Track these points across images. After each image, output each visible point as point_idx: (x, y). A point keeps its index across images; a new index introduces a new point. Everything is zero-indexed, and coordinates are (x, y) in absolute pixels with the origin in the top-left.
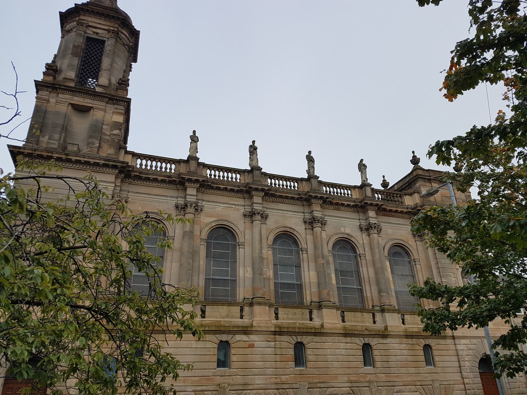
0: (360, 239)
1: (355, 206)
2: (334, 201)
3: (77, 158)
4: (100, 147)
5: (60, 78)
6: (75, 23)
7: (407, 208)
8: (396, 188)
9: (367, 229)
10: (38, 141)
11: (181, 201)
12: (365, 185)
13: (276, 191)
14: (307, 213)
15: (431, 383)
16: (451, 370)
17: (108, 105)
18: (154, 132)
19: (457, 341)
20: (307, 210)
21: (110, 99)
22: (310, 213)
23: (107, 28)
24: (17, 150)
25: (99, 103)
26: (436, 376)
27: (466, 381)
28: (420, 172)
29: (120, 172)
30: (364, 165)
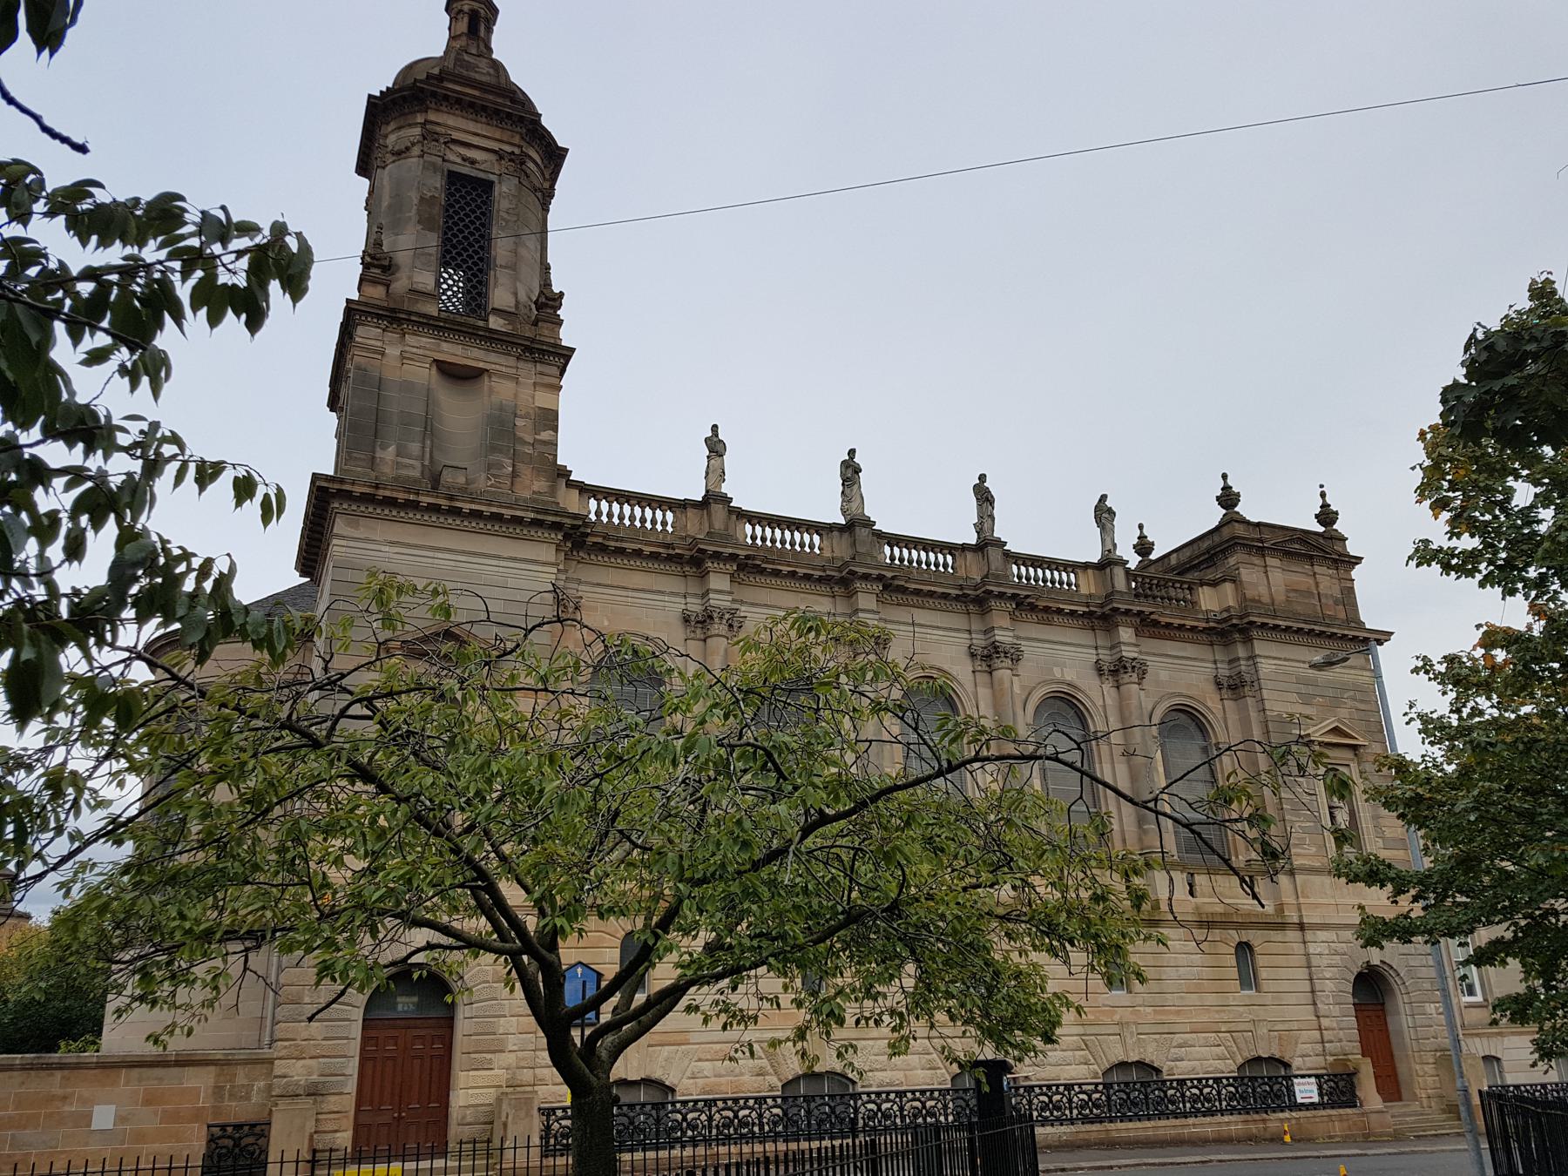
0: (1097, 695)
1: (1089, 615)
2: (1041, 604)
3: (474, 507)
4: (514, 475)
5: (400, 284)
6: (417, 131)
7: (1207, 621)
8: (1173, 560)
9: (1114, 672)
10: (374, 458)
11: (695, 606)
12: (1109, 562)
13: (908, 580)
14: (977, 632)
15: (1250, 1026)
16: (1292, 999)
17: (521, 364)
18: (618, 431)
19: (1309, 935)
20: (976, 625)
21: (527, 349)
22: (985, 632)
23: (495, 146)
24: (337, 486)
25: (502, 359)
26: (1261, 1013)
27: (1325, 1022)
28: (1240, 530)
29: (566, 537)
30: (1111, 512)
